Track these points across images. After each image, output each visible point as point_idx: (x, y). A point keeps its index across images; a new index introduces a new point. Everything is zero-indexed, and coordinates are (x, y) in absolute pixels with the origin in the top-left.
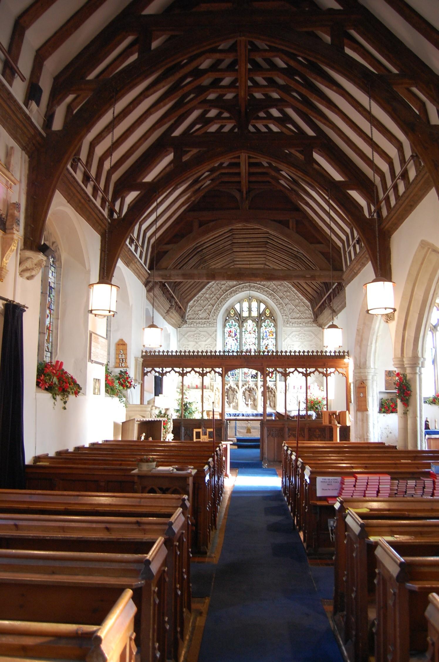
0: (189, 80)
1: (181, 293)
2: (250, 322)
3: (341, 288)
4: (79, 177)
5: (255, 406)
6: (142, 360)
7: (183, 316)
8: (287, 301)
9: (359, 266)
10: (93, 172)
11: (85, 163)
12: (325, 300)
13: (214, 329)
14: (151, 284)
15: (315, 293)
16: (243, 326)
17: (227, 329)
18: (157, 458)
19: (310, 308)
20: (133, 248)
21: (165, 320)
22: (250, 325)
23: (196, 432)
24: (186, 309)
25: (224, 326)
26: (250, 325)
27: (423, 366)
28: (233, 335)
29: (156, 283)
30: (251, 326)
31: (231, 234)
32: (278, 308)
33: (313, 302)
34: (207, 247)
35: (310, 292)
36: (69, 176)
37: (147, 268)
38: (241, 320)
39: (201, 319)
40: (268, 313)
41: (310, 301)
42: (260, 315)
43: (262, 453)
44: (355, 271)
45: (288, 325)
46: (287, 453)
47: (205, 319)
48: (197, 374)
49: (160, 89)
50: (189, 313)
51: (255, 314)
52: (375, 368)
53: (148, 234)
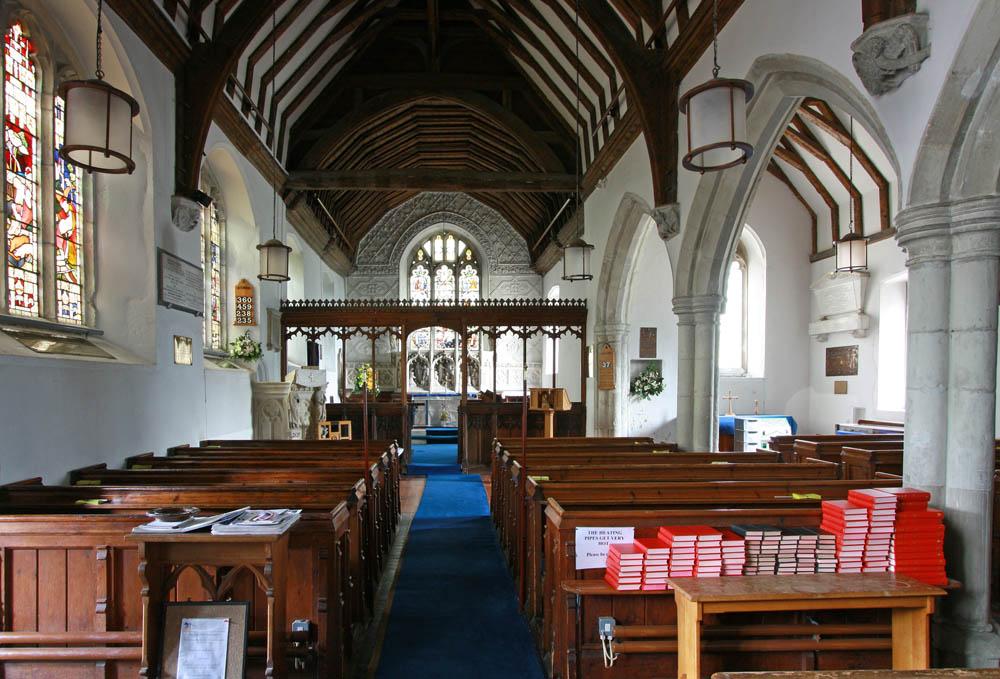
0: (377, 21)
1: (347, 222)
2: (444, 267)
3: (576, 205)
4: (237, 104)
5: (452, 386)
6: (280, 314)
7: (352, 259)
8: (494, 237)
9: (611, 158)
10: (254, 98)
11: (243, 85)
12: (549, 233)
13: (395, 277)
14: (292, 196)
15: (534, 224)
16: (435, 274)
17: (413, 279)
18: (89, 528)
19: (526, 248)
20: (251, 122)
21: (324, 261)
22: (445, 273)
23: (342, 426)
24: (356, 251)
25: (410, 274)
26: (445, 273)
27: (723, 311)
28: (422, 287)
29: (300, 195)
30: (447, 275)
31: (415, 125)
32: (484, 247)
33: (530, 238)
34: (381, 146)
35: (527, 222)
36: (161, 22)
37: (282, 166)
38: (432, 267)
39: (378, 263)
40: (469, 254)
41: (527, 237)
42: (458, 259)
43: (461, 451)
44: (604, 169)
45: (496, 272)
46: (501, 460)
47: (383, 263)
48: (366, 336)
49: (343, 35)
50: (360, 255)
51: (451, 257)
52: (627, 324)
53: (282, 106)
